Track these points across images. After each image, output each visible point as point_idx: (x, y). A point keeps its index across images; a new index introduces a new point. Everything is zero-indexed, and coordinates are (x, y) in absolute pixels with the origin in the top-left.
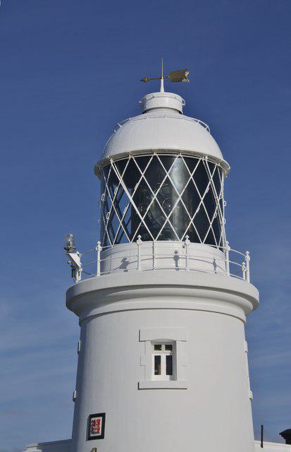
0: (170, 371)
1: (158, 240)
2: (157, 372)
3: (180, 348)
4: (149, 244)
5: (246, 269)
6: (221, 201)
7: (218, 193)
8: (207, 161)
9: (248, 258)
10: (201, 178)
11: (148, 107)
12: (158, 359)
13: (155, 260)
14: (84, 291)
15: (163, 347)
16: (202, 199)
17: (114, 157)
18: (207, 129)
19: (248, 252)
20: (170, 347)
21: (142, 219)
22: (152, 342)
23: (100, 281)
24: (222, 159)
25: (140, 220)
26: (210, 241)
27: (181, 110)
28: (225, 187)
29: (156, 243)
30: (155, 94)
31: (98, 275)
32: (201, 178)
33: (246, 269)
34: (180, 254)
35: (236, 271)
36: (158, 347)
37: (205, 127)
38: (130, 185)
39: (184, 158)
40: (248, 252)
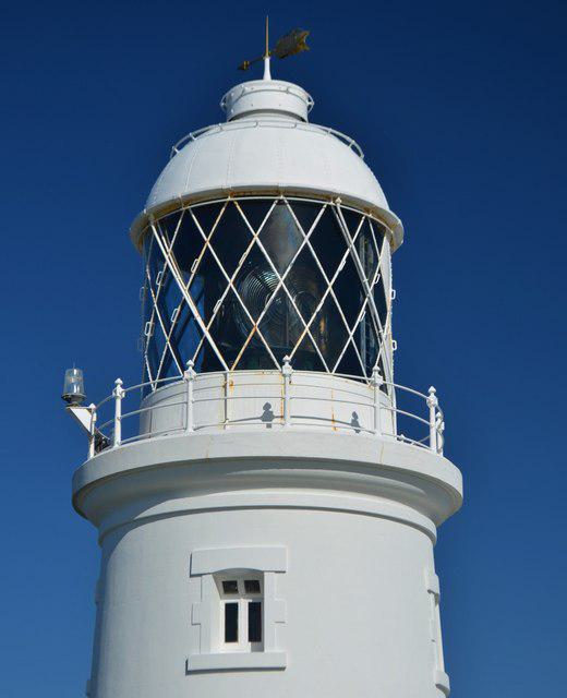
0: (256, 634)
1: (240, 367)
2: (231, 635)
3: (271, 586)
4: (214, 378)
5: (436, 423)
6: (379, 289)
7: (383, 323)
8: (339, 206)
9: (432, 400)
10: (329, 241)
11: (234, 112)
12: (231, 611)
13: (229, 402)
14: (97, 477)
15: (241, 587)
16: (330, 284)
17: (158, 211)
18: (354, 148)
19: (432, 389)
20: (254, 585)
21: (206, 330)
22: (216, 575)
23: (124, 455)
24: (387, 208)
25: (202, 333)
26: (350, 368)
27: (304, 114)
28: (393, 310)
29: (235, 376)
30: (247, 86)
31: (116, 446)
32: (329, 241)
33: (436, 423)
34: (276, 410)
35: (411, 428)
36: (229, 587)
37: (347, 143)
38: (184, 267)
39: (291, 202)
40: (432, 389)
